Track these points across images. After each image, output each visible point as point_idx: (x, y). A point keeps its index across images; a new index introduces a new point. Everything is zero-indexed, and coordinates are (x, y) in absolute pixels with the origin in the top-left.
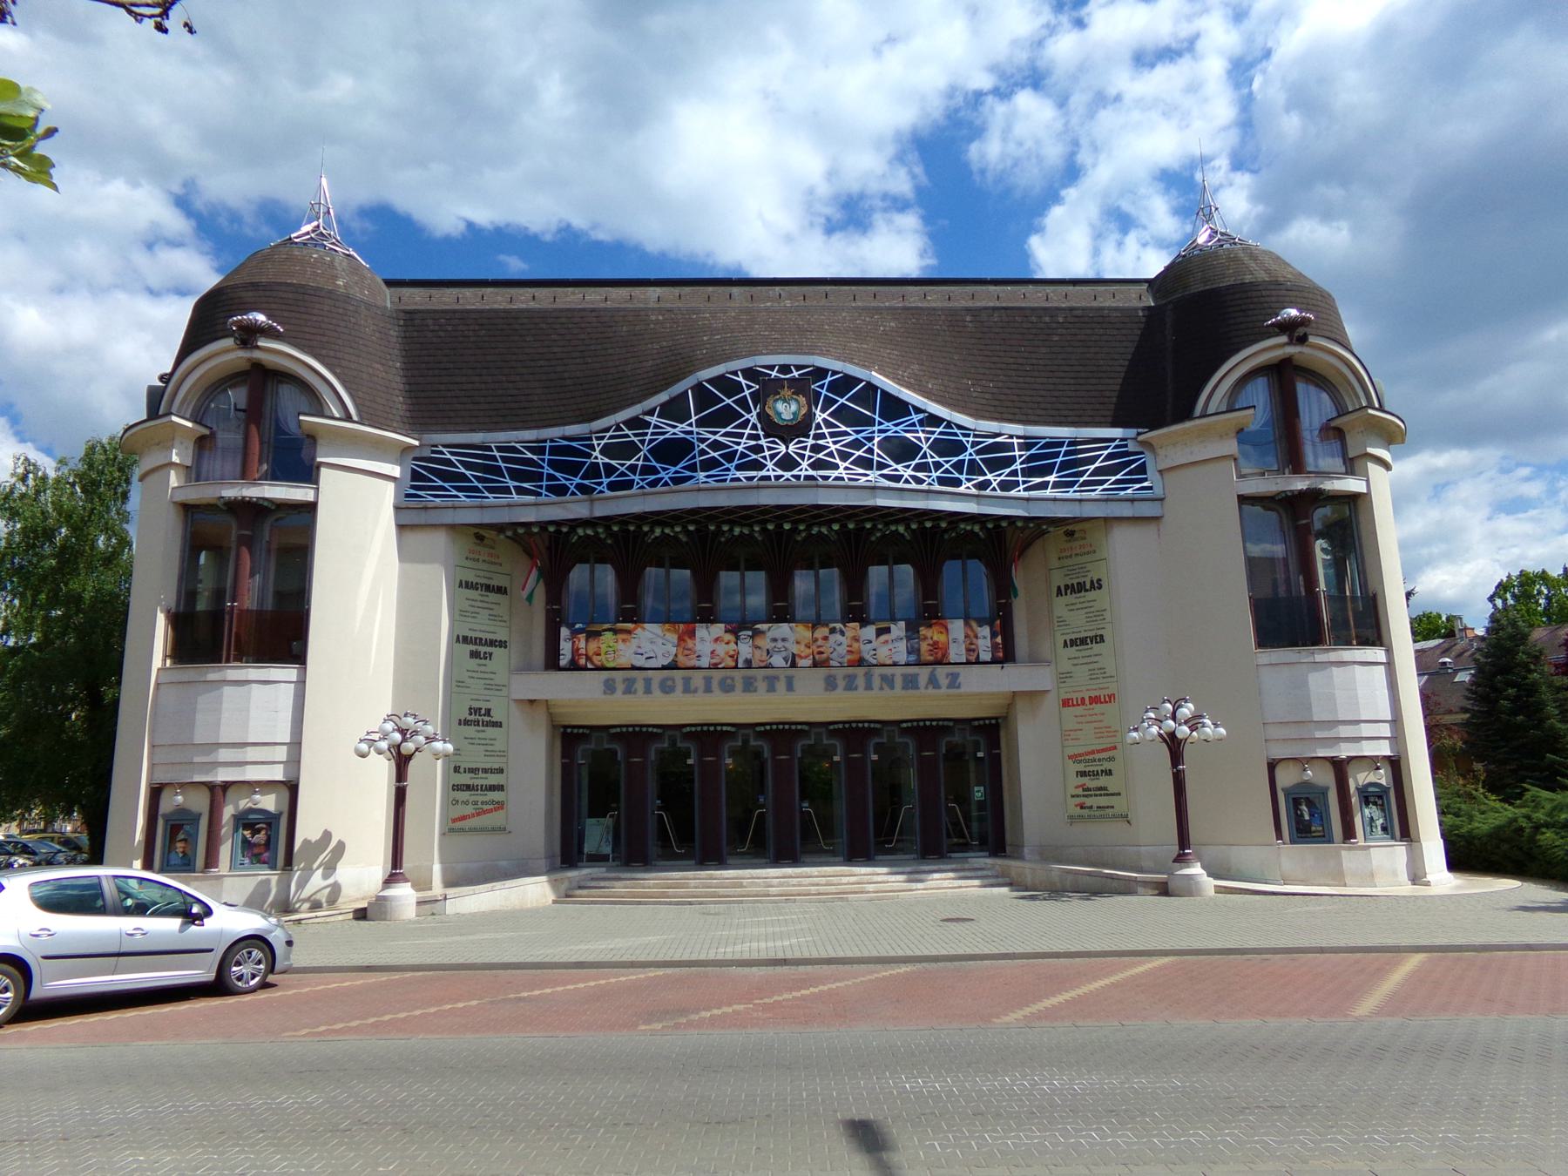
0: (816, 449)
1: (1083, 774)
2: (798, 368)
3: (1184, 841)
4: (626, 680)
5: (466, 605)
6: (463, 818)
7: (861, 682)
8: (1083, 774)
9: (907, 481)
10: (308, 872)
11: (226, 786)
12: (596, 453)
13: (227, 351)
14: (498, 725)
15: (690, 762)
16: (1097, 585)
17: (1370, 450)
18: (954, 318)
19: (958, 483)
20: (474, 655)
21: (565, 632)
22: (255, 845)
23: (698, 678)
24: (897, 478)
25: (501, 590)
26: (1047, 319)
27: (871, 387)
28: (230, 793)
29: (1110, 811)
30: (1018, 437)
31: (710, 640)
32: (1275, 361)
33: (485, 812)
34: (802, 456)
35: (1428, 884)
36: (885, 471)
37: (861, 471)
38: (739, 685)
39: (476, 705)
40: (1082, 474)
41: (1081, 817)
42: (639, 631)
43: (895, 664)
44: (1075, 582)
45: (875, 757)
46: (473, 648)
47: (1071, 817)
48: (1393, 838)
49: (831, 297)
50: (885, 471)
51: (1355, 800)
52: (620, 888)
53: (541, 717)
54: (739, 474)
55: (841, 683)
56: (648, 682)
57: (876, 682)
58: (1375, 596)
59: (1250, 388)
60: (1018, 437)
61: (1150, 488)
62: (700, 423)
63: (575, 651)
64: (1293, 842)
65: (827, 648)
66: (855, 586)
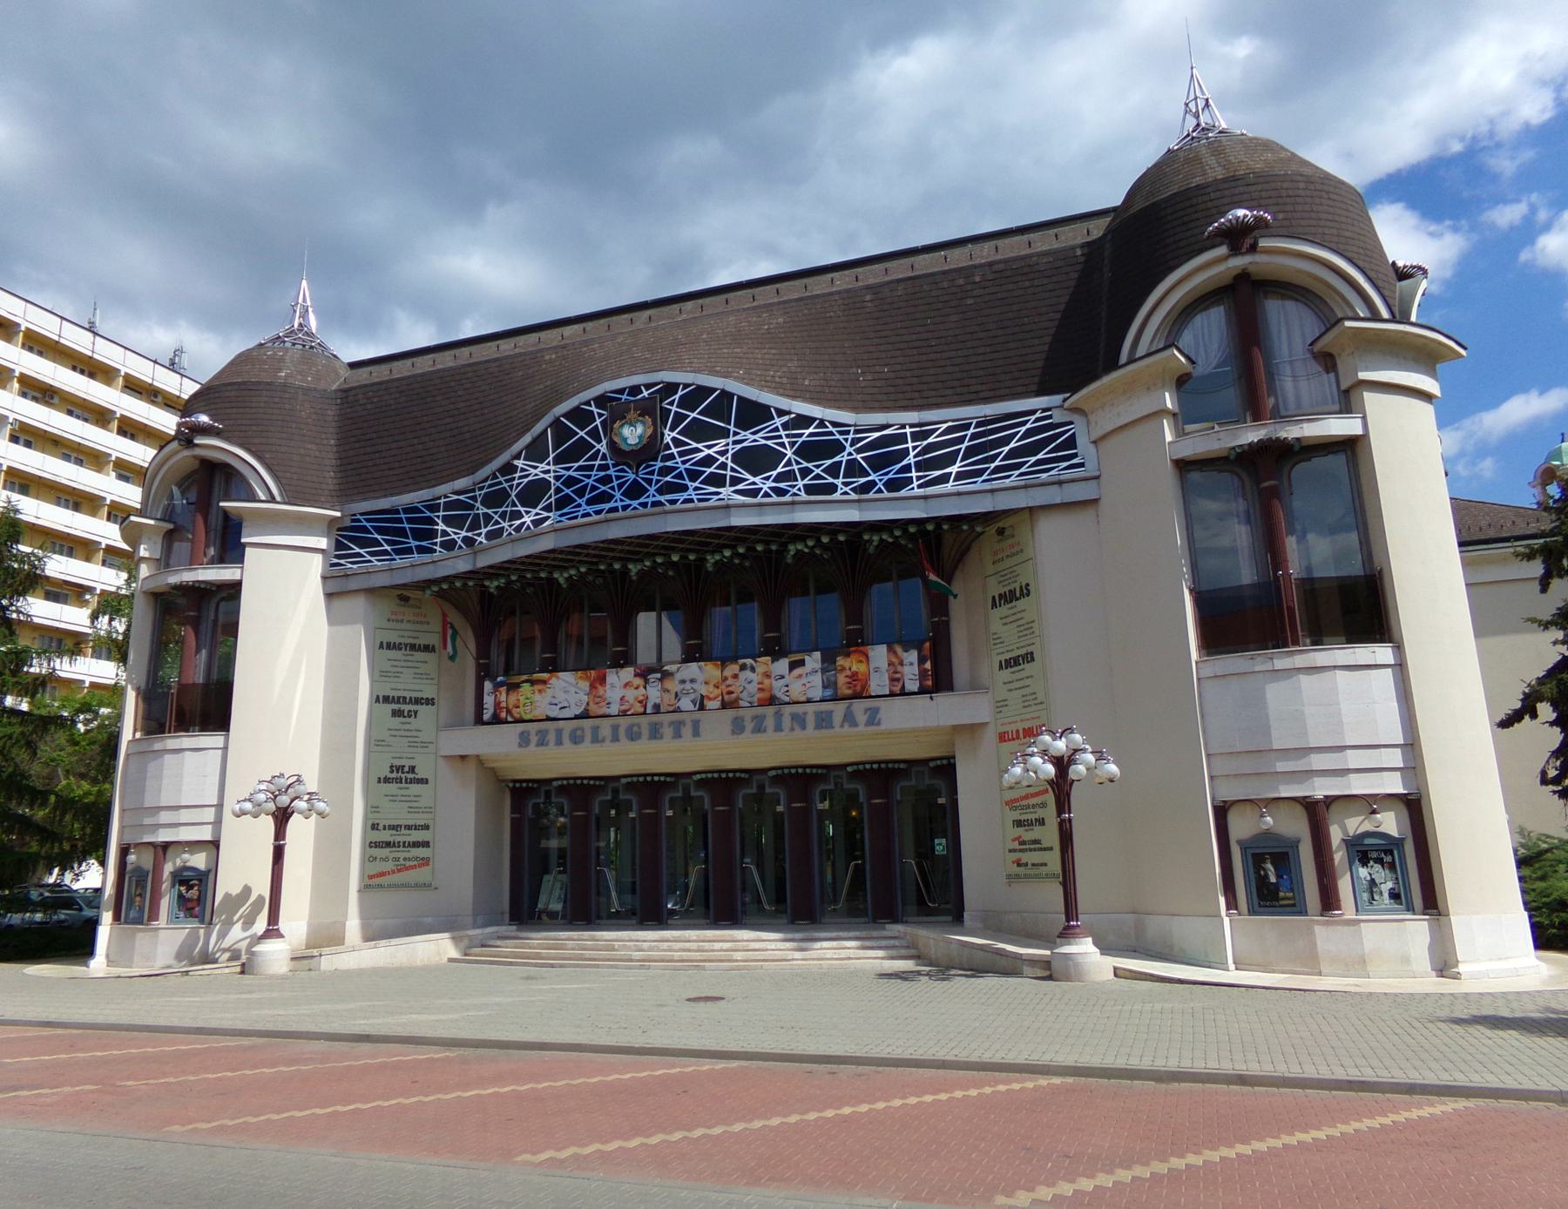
0: (665, 471)
1: (1018, 823)
2: (648, 387)
3: (1071, 910)
4: (539, 732)
5: (387, 666)
6: (382, 874)
7: (770, 722)
8: (1018, 823)
9: (767, 495)
10: (229, 924)
11: (166, 846)
12: (478, 505)
13: (176, 452)
14: (424, 781)
15: (780, 809)
16: (1025, 591)
17: (1363, 375)
18: (850, 298)
19: (832, 489)
20: (396, 713)
21: (488, 686)
22: (189, 900)
23: (605, 726)
24: (753, 493)
25: (427, 648)
26: (961, 282)
27: (726, 396)
28: (170, 852)
29: (1043, 870)
30: (912, 426)
31: (620, 684)
32: (1227, 280)
33: (407, 868)
34: (649, 482)
35: (1457, 976)
36: (740, 487)
37: (713, 489)
38: (645, 732)
39: (398, 763)
40: (993, 458)
41: (1018, 876)
42: (553, 681)
43: (809, 701)
44: (1007, 589)
45: (670, 813)
46: (396, 707)
47: (1009, 876)
48: (1410, 908)
49: (732, 303)
50: (740, 487)
51: (1339, 856)
52: (508, 947)
53: (471, 770)
54: (590, 509)
55: (749, 726)
56: (559, 732)
57: (787, 721)
58: (1380, 572)
59: (1199, 320)
60: (912, 426)
61: (1082, 465)
62: (557, 461)
63: (497, 705)
64: (1252, 912)
65: (736, 686)
66: (773, 620)
